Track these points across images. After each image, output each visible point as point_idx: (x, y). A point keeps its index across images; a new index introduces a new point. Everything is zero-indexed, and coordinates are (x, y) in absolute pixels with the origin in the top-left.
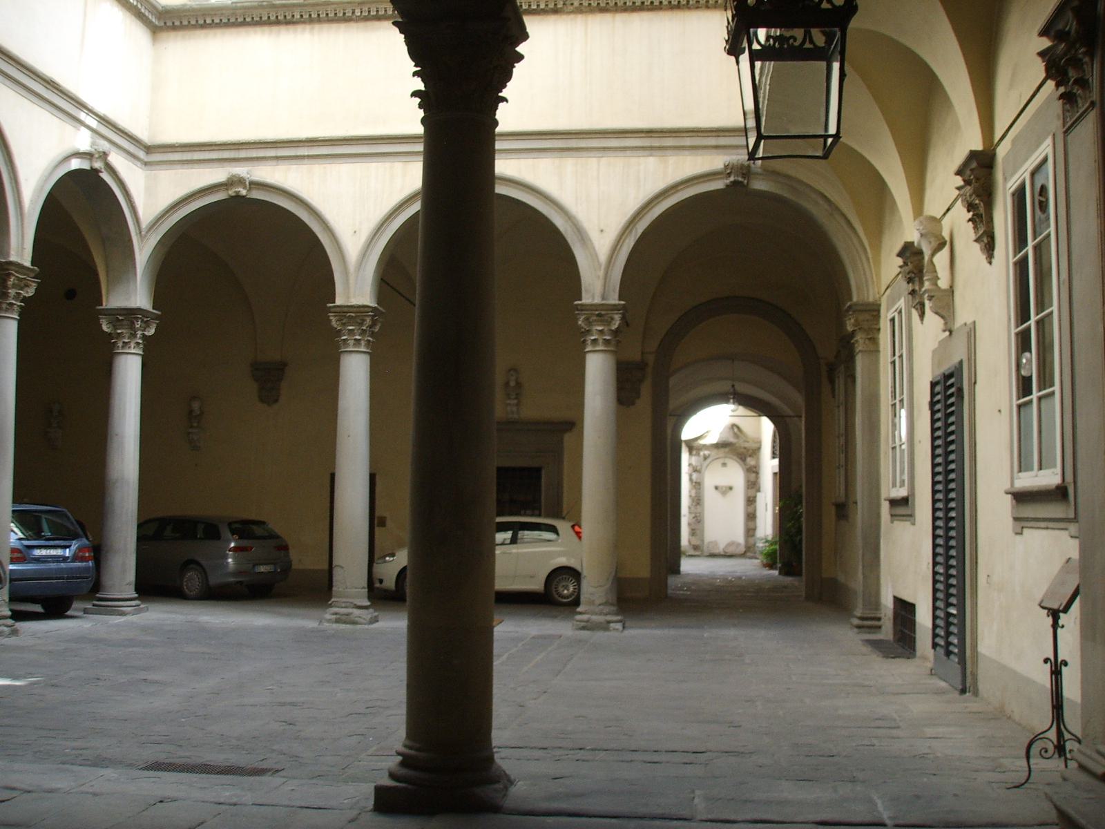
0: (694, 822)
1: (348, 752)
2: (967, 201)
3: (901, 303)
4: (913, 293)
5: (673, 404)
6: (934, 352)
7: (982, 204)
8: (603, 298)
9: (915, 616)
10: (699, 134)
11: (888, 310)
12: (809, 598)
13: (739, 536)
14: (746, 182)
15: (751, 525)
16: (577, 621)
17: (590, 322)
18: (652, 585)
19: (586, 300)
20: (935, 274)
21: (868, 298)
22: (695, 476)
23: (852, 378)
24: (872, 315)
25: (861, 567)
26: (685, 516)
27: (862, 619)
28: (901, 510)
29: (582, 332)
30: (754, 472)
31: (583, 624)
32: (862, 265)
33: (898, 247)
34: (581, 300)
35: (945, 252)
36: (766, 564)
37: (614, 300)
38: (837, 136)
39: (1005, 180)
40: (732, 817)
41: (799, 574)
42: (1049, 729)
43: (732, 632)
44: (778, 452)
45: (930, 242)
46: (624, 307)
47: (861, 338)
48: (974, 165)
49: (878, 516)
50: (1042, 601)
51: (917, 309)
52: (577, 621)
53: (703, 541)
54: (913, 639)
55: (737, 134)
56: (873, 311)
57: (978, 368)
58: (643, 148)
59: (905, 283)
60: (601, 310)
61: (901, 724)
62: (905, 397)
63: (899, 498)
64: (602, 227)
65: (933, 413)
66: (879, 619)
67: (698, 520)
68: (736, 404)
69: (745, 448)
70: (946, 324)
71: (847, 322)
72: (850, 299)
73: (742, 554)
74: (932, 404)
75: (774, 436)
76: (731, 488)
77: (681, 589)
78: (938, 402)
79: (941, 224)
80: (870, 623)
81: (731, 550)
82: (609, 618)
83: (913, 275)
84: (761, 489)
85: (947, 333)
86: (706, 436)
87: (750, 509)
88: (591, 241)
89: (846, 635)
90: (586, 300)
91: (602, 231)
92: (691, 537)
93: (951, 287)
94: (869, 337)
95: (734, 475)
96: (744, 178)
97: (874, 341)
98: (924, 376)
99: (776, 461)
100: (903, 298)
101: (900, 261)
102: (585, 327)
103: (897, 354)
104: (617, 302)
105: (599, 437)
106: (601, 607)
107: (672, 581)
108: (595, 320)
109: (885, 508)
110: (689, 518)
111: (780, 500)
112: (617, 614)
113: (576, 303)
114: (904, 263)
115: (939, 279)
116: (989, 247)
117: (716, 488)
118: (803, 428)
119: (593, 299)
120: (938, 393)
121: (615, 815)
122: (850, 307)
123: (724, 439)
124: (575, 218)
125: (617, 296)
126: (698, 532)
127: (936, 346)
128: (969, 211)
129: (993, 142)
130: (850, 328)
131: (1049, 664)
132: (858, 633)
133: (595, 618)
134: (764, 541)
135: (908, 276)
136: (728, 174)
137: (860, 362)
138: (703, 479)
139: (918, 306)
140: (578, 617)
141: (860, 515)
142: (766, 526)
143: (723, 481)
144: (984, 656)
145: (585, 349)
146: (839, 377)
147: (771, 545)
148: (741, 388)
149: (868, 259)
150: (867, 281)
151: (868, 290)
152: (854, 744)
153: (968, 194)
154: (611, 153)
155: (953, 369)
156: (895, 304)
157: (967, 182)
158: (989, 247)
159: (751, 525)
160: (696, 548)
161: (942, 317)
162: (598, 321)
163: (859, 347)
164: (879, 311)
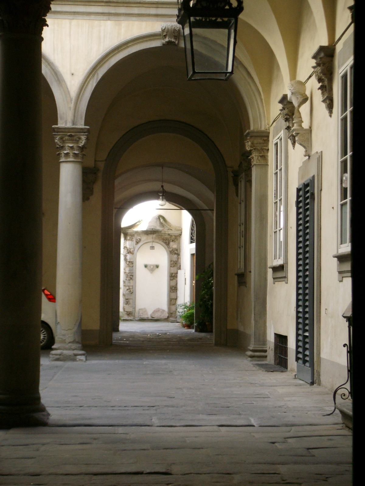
0: (153, 427)
2: (319, 76)
3: (282, 134)
4: (288, 128)
5: (118, 197)
6: (300, 168)
7: (326, 80)
8: (73, 124)
9: (287, 345)
10: (145, 5)
11: (274, 138)
12: (217, 344)
13: (163, 304)
14: (177, 42)
16: (53, 355)
17: (63, 141)
18: (102, 337)
19: (61, 124)
20: (300, 119)
21: (261, 128)
22: (129, 256)
23: (250, 181)
24: (264, 140)
25: (253, 315)
27: (254, 351)
28: (280, 274)
29: (58, 148)
30: (175, 254)
31: (58, 357)
32: (257, 100)
33: (280, 97)
34: (57, 125)
35: (308, 103)
36: (186, 324)
37: (81, 125)
38: (232, 73)
39: (339, 67)
40: (174, 424)
41: (211, 331)
42: (346, 383)
43: (163, 362)
44: (195, 238)
45: (298, 98)
46: (88, 131)
47: (255, 156)
48: (322, 55)
49: (266, 279)
50: (343, 314)
51: (291, 139)
52: (53, 355)
53: (135, 308)
54: (286, 360)
55: (171, 6)
56: (265, 136)
57: (323, 182)
58: (103, 14)
59: (284, 121)
60: (73, 132)
61: (270, 396)
62: (283, 197)
63: (278, 266)
64: (73, 72)
65: (298, 208)
66: (265, 351)
67: (131, 291)
68: (164, 200)
69: (169, 235)
70: (306, 151)
71: (246, 144)
72: (249, 128)
73: (165, 319)
74: (298, 203)
75: (192, 225)
76: (157, 267)
77: (121, 340)
78: (301, 201)
79: (305, 86)
80: (259, 355)
81: (157, 316)
82: (76, 352)
83: (288, 117)
85: (307, 157)
86: (138, 225)
87: (173, 283)
88: (64, 81)
89: (243, 363)
90: (61, 124)
91: (73, 74)
92: (125, 305)
93: (310, 128)
94: (261, 155)
95: (160, 256)
96: (176, 39)
97: (264, 157)
98: (294, 184)
99: (194, 245)
100: (283, 130)
101: (280, 106)
102: (60, 144)
103: (279, 168)
104: (83, 127)
105: (69, 223)
106: (70, 344)
107: (115, 335)
108: (68, 140)
109: (270, 271)
111: (196, 275)
112: (83, 350)
113: (53, 126)
114: (283, 108)
115: (303, 122)
116: (330, 107)
117: (146, 266)
118: (214, 218)
119: (66, 124)
120: (301, 196)
121: (111, 425)
122: (248, 134)
123: (152, 227)
124: (52, 64)
125: (83, 122)
126: (131, 301)
127: (301, 165)
128: (319, 83)
129: (335, 41)
130: (248, 148)
131: (346, 347)
132: (251, 361)
133: (65, 352)
134: (183, 307)
135: (285, 117)
136: (164, 36)
137: (255, 172)
138: (136, 259)
139: (291, 137)
140: (53, 352)
141: (253, 278)
142: (185, 295)
143: (152, 262)
144: (324, 358)
145: (59, 159)
146: (241, 181)
147: (190, 310)
148: (168, 188)
149: (261, 100)
150: (260, 115)
151: (261, 121)
152: (241, 403)
153: (319, 72)
154: (80, 17)
155: (309, 181)
156: (277, 135)
157: (318, 65)
158: (330, 107)
159: (173, 295)
160: (129, 314)
161: (304, 147)
162: (70, 140)
163: (254, 162)
164: (268, 137)
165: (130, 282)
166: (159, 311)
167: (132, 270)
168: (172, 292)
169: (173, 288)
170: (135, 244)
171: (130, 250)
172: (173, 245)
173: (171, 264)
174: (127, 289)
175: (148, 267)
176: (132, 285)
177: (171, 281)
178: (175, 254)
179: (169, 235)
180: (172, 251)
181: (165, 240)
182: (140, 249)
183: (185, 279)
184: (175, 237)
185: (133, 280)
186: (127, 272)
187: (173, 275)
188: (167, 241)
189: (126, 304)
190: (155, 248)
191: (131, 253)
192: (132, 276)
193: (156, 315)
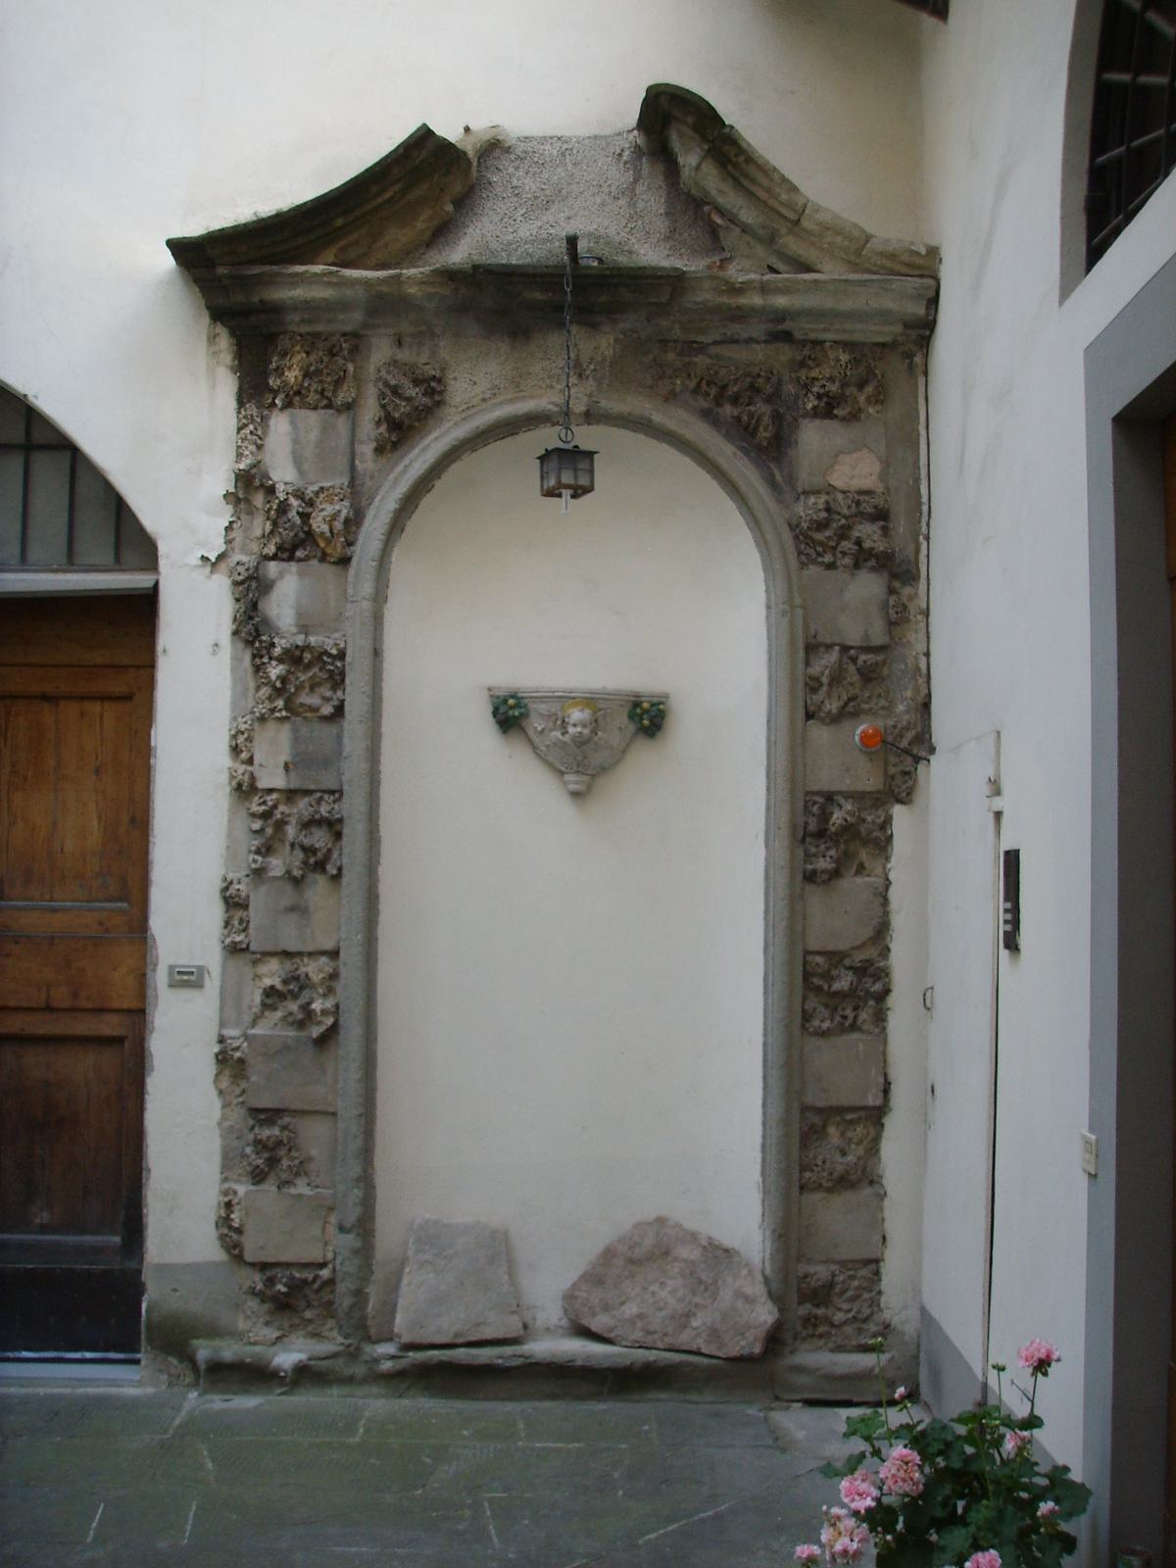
1: (377, 504)
15: (836, 1068)
22: (288, 596)
26: (188, 979)
30: (863, 557)
52: (710, 357)
67: (314, 1035)
76: (648, 718)
81: (647, 1316)
84: (919, 797)
110: (229, 998)
117: (510, 715)
126: (314, 1137)
143: (575, 655)
160: (291, 1294)
165: (299, 910)
166: (662, 1253)
167: (331, 760)
168: (823, 1034)
169: (843, 982)
170: (367, 449)
171: (305, 517)
172: (839, 460)
173: (813, 685)
174: (270, 992)
175: (536, 724)
176: (329, 945)
177: (815, 898)
178: (857, 566)
179: (786, 337)
180: (821, 526)
181: (735, 400)
182: (426, 502)
183: (1012, 860)
184: (855, 361)
185: (337, 878)
186: (272, 777)
187: (837, 817)
188: (761, 408)
189: (258, 1177)
190: (604, 475)
191: (324, 558)
192: (334, 827)
193: (631, 1309)
